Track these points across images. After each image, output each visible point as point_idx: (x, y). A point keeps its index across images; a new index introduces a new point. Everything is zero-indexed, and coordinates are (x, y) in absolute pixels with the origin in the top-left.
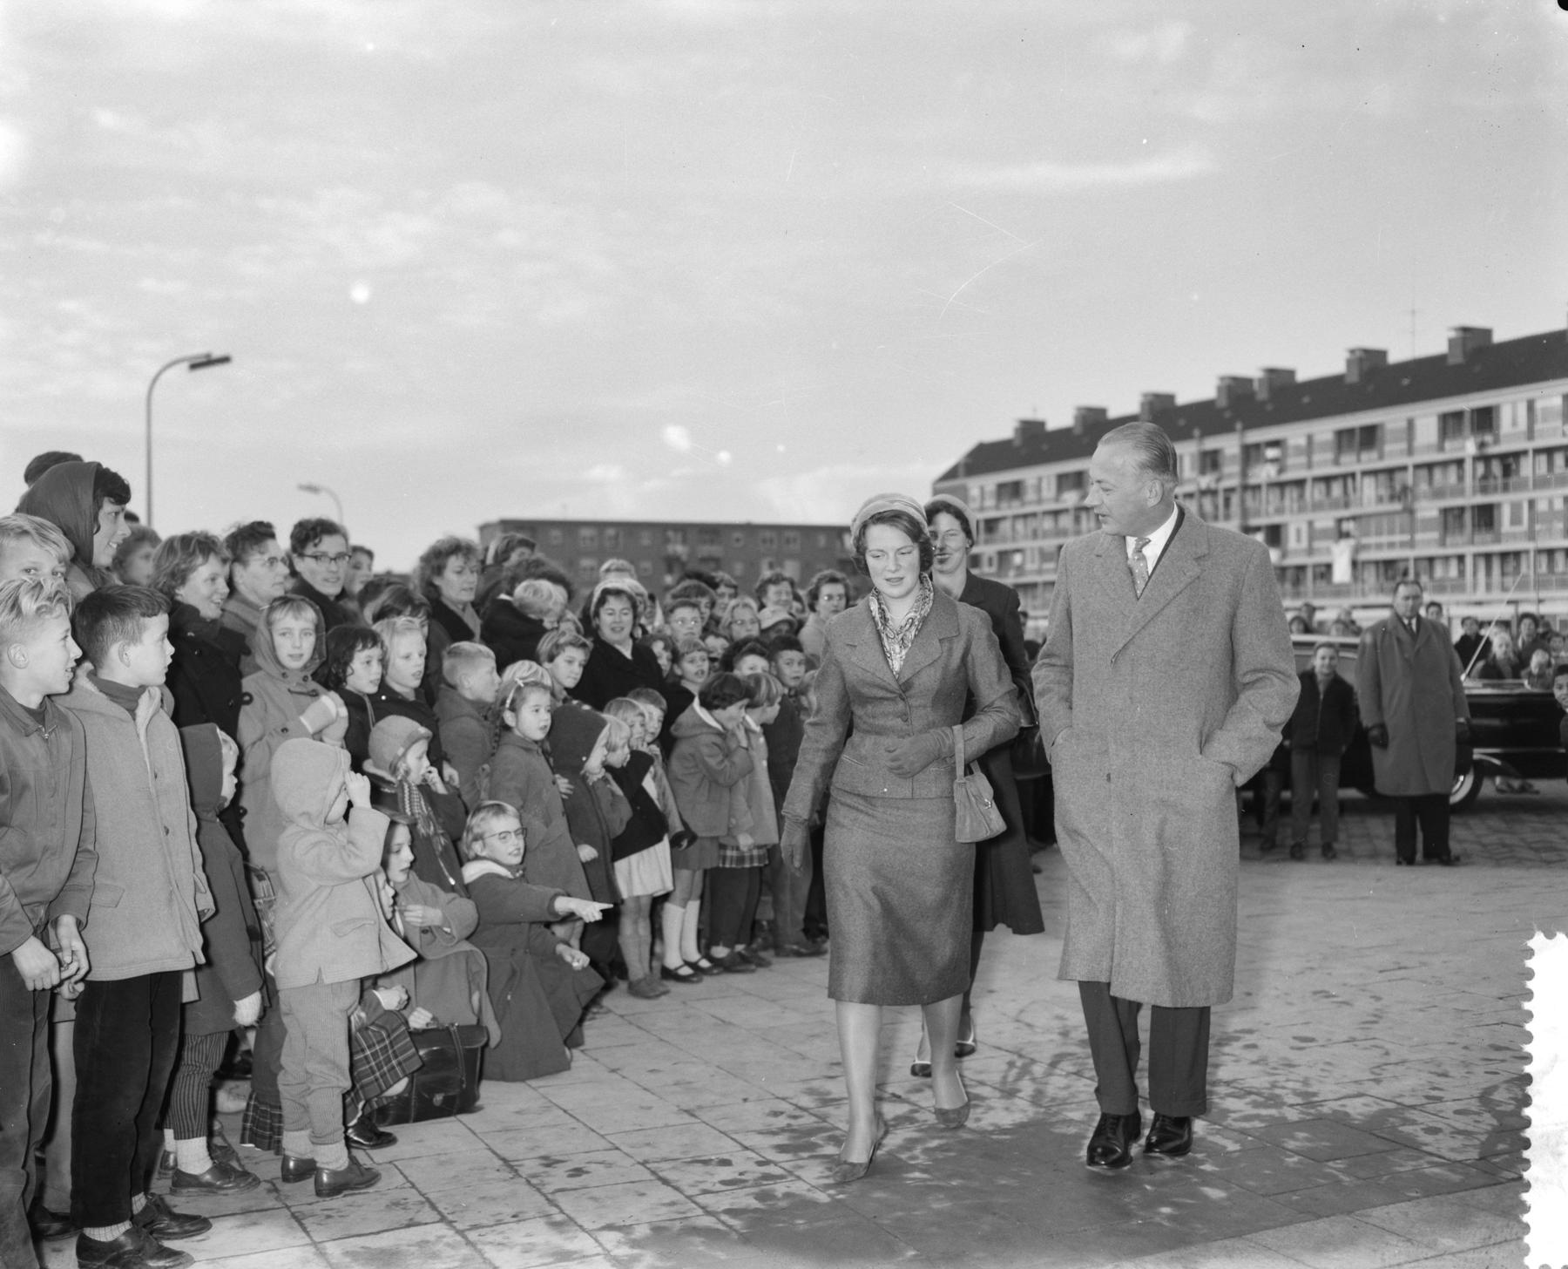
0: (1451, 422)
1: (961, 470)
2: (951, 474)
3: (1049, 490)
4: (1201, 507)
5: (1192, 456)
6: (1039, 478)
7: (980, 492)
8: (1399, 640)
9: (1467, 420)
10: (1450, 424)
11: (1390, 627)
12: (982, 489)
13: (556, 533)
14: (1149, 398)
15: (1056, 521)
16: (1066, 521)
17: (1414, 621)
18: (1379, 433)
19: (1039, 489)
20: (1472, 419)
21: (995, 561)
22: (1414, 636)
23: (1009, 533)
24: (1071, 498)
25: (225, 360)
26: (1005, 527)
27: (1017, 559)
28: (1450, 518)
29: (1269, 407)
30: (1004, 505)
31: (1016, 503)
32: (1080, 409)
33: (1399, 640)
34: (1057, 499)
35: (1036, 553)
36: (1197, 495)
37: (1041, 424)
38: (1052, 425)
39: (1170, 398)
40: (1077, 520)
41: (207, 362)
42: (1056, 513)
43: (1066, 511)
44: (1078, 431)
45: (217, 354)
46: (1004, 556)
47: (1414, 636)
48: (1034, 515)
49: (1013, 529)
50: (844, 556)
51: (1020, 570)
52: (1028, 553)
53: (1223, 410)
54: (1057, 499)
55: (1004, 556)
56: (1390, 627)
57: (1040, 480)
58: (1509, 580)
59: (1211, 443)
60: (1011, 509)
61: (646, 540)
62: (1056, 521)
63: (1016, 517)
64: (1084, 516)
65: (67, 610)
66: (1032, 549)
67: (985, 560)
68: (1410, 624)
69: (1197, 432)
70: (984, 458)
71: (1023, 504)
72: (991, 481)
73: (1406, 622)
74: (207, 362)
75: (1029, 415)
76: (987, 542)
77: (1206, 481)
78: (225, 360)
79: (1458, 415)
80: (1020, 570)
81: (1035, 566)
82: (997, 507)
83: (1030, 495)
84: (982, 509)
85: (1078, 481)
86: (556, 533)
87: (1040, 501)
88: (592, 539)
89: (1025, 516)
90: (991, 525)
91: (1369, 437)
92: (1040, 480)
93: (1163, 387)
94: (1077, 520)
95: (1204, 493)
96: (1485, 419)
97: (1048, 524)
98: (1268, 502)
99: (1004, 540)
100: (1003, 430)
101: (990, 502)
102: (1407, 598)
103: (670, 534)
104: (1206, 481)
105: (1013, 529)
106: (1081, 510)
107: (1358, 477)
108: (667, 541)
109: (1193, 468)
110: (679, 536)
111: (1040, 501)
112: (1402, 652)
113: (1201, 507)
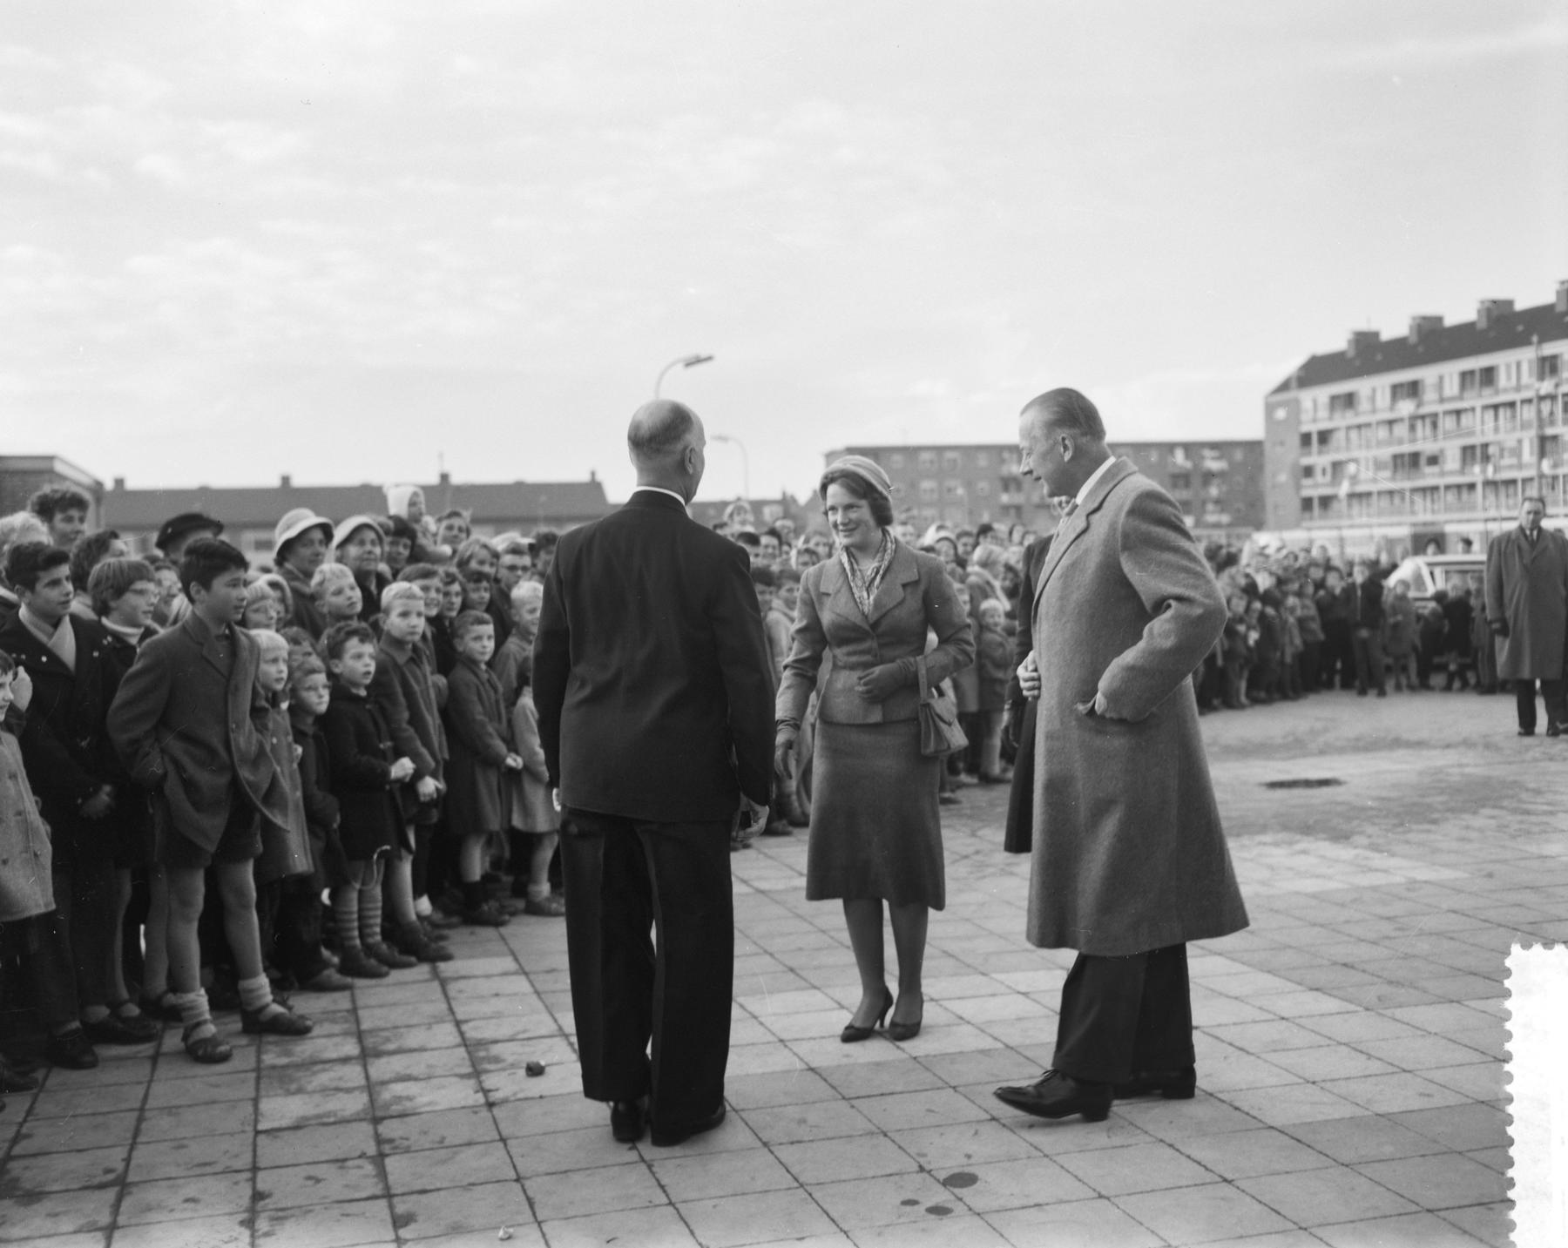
0: (1468, 377)
1: (1294, 384)
2: (1284, 387)
3: (1384, 398)
4: (1539, 412)
5: (1530, 362)
6: (1374, 389)
7: (1314, 403)
8: (1519, 548)
9: (1477, 377)
10: (1397, 391)
11: (1513, 537)
12: (1315, 402)
13: (897, 458)
14: (1418, 321)
15: (1391, 431)
16: (1401, 430)
17: (1535, 533)
18: (1420, 387)
19: (1373, 399)
20: (1481, 376)
21: (1329, 471)
22: (1533, 544)
23: (1343, 443)
24: (1406, 407)
25: (709, 358)
26: (1339, 437)
27: (1352, 468)
28: (1399, 461)
29: (1421, 349)
30: (1337, 415)
31: (1487, 391)
32: (1414, 318)
33: (1519, 548)
34: (1392, 408)
35: (1371, 463)
36: (1535, 401)
37: (1376, 335)
38: (1386, 336)
39: (1509, 303)
40: (1412, 428)
41: (698, 360)
42: (1391, 423)
43: (1400, 420)
44: (1483, 325)
45: (704, 354)
46: (1337, 466)
47: (1533, 544)
48: (1368, 425)
49: (1348, 439)
50: (1177, 471)
51: (1354, 479)
52: (1363, 463)
53: (1415, 346)
54: (1392, 408)
55: (1337, 466)
56: (1513, 537)
57: (1441, 378)
58: (1511, 502)
59: (1549, 349)
60: (1343, 420)
61: (983, 461)
62: (1391, 431)
63: (1349, 428)
64: (1419, 424)
65: (1453, 766)
66: (1367, 460)
67: (1318, 472)
68: (1531, 534)
69: (1535, 339)
70: (1317, 371)
71: (1497, 392)
72: (1323, 393)
73: (1528, 532)
74: (698, 360)
75: (1363, 326)
76: (1320, 453)
77: (1546, 387)
78: (709, 358)
79: (1472, 373)
80: (1354, 479)
81: (1370, 474)
82: (1331, 418)
83: (1364, 405)
84: (1315, 420)
85: (1413, 389)
86: (897, 459)
87: (1374, 411)
88: (932, 462)
89: (1359, 427)
90: (1324, 437)
91: (1349, 400)
92: (1374, 390)
93: (1430, 310)
94: (1412, 428)
95: (1541, 398)
96: (1488, 375)
97: (1383, 433)
98: (1483, 423)
99: (1338, 450)
100: (1336, 341)
101: (1323, 413)
102: (1529, 513)
103: (1006, 455)
104: (1546, 387)
105: (1348, 439)
106: (1414, 419)
107: (1518, 404)
108: (1003, 461)
109: (1530, 375)
110: (1015, 456)
111: (1374, 411)
112: (1521, 557)
113: (1539, 412)
